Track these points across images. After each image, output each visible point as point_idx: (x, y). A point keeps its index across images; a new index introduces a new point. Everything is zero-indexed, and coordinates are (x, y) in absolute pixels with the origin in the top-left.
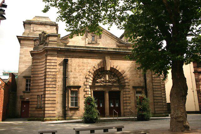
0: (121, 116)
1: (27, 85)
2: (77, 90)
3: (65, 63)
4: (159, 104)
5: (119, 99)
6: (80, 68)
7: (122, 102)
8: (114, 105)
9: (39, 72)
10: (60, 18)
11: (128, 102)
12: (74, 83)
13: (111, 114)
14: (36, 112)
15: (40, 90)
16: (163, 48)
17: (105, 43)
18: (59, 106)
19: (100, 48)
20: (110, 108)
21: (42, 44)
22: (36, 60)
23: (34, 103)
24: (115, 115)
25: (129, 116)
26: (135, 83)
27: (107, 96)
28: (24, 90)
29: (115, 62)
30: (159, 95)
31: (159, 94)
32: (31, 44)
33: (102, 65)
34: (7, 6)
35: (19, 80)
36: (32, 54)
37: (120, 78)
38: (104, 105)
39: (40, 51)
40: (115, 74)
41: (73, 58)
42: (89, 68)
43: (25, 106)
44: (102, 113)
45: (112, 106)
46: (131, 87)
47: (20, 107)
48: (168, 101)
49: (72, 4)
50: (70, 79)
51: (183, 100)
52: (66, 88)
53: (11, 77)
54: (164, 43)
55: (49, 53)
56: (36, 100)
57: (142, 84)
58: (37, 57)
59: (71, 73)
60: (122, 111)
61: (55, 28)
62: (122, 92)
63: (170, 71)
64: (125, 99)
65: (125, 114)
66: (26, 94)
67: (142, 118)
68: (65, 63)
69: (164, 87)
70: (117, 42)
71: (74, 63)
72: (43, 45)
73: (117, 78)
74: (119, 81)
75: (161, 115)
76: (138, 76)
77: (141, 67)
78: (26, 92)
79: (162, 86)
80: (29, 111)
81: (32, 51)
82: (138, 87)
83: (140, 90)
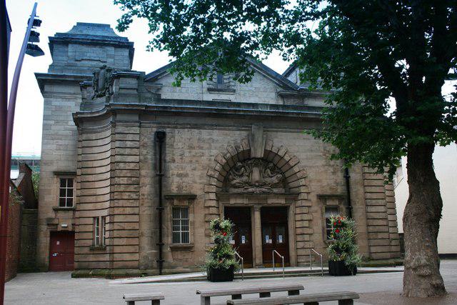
0: (252, 267)
1: (62, 193)
3: (160, 138)
4: (380, 236)
5: (285, 224)
6: (194, 152)
7: (291, 232)
8: (274, 238)
9: (96, 164)
10: (155, 44)
11: (306, 231)
12: (179, 187)
13: (267, 261)
14: (91, 258)
15: (99, 206)
16: (388, 115)
17: (256, 93)
18: (146, 242)
19: (239, 104)
20: (265, 246)
21: (102, 96)
22: (87, 133)
23: (85, 236)
24: (278, 263)
25: (308, 266)
26: (323, 187)
27: (257, 217)
28: (57, 204)
29: (276, 137)
30: (382, 215)
32: (70, 94)
33: (244, 145)
34: (41, 22)
35: (45, 181)
36: (79, 120)
37: (287, 174)
38: (249, 239)
39: (98, 112)
40: (275, 165)
41: (176, 128)
42: (214, 152)
43: (58, 243)
44: (249, 262)
45: (269, 241)
46: (313, 197)
47: (48, 245)
48: (401, 230)
49: (181, 7)
50: (171, 179)
51: (430, 229)
53: (23, 175)
54: (392, 103)
55: (119, 117)
56: (90, 228)
57: (340, 190)
58: (90, 127)
59: (172, 165)
60: (292, 253)
61: (126, 53)
62: (292, 207)
63: (404, 160)
64: (298, 224)
65: (299, 261)
66: (61, 214)
67: (340, 269)
69: (393, 196)
70: (278, 85)
72: (104, 99)
73: (279, 175)
74: (284, 182)
76: (332, 170)
77: (340, 157)
78: (61, 210)
79: (387, 193)
80: (73, 253)
81: (77, 113)
82: (331, 197)
83: (336, 203)
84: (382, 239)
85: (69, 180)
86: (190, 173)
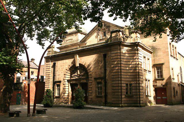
2: (59, 84)
3: (54, 66)
6: (62, 67)
12: (58, 79)
31: (117, 84)
43: (163, 93)
46: (93, 79)
52: (54, 83)
57: (102, 76)
68: (54, 66)
71: (59, 63)
75: (117, 105)
76: (100, 67)
83: (100, 80)
84: (117, 95)
85: (160, 67)
86: (61, 74)
